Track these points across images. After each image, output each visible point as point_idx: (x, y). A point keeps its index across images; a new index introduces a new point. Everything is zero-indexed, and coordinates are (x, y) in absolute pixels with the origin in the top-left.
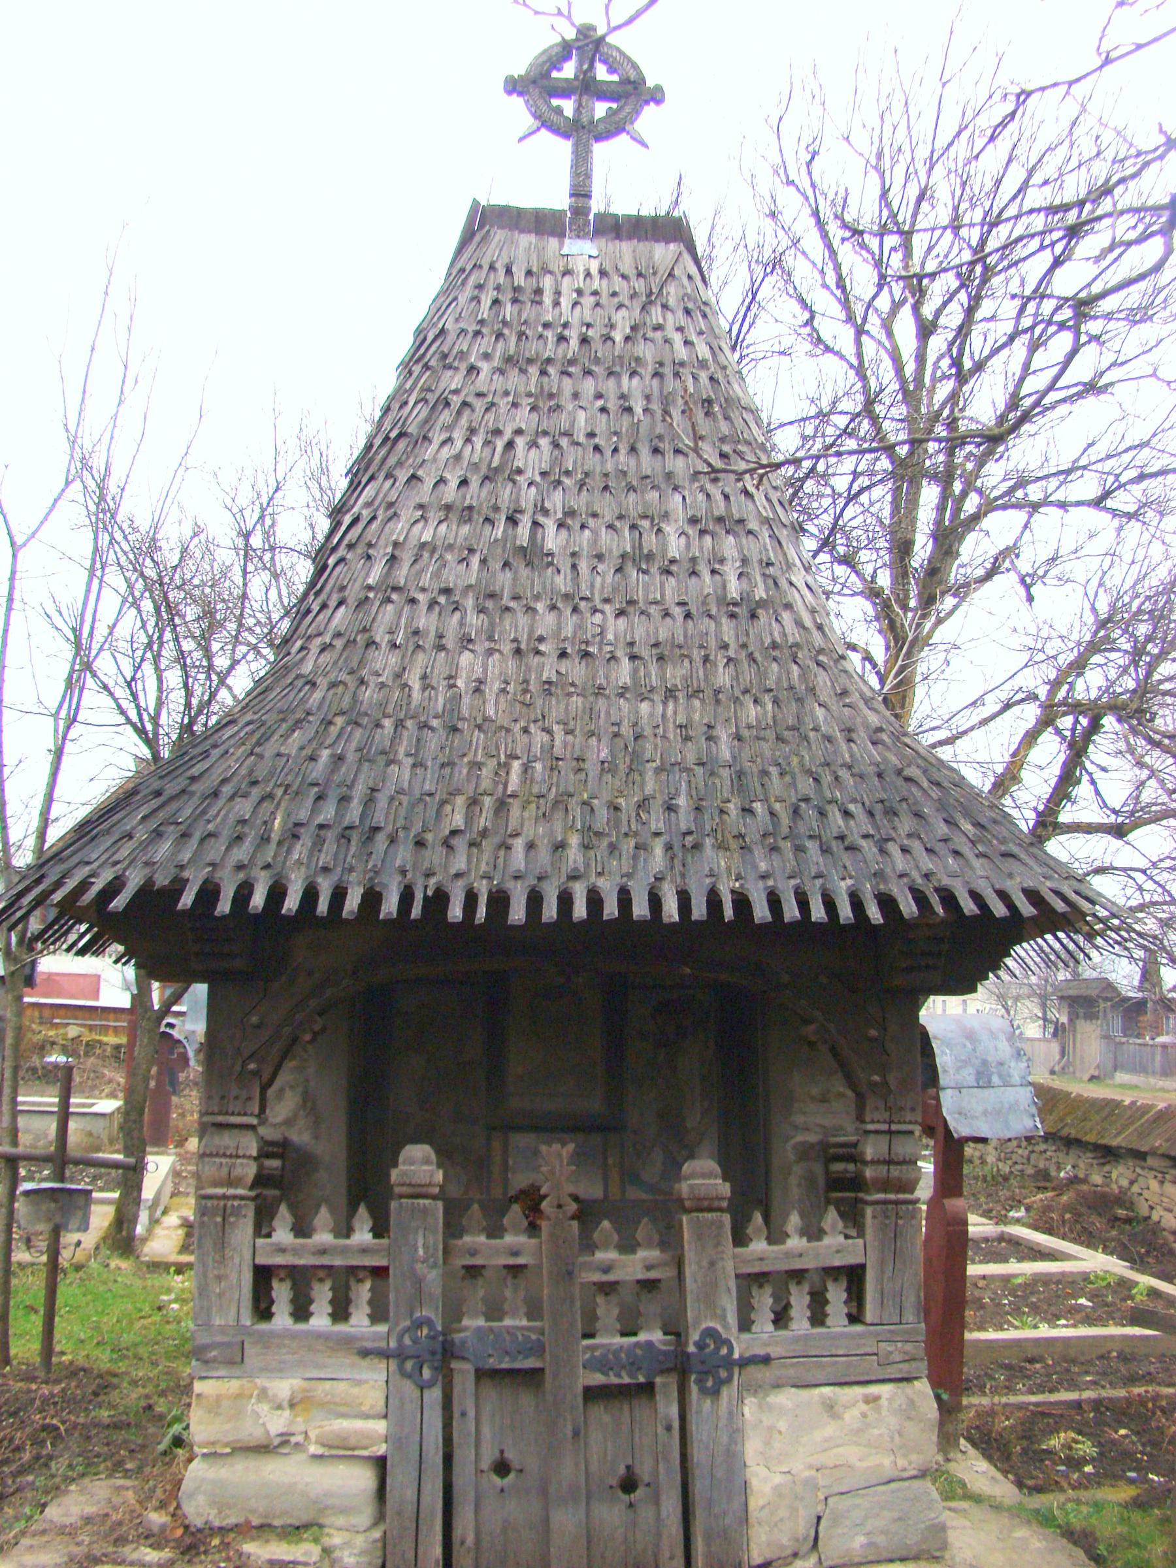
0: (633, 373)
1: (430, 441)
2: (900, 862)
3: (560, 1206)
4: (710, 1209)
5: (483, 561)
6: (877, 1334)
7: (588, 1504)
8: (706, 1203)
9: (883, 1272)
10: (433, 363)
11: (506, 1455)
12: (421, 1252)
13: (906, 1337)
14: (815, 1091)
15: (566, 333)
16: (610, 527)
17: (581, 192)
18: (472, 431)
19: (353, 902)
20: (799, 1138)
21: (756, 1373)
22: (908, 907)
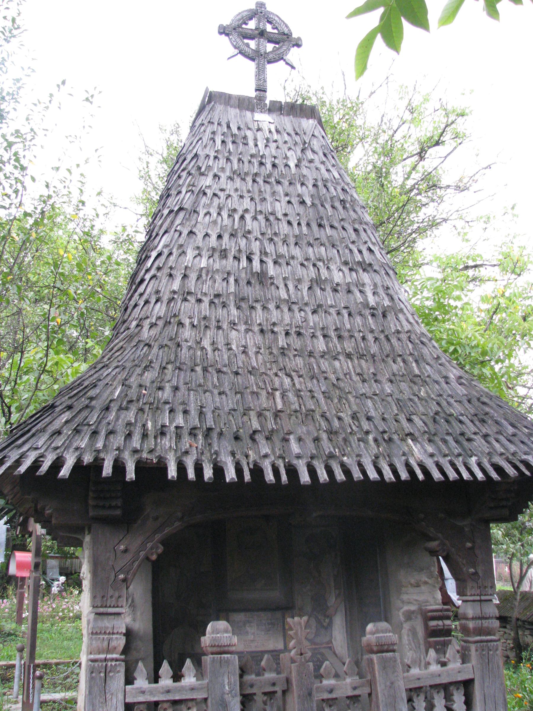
0: (302, 184)
4: (387, 651)
5: (236, 281)
8: (386, 647)
10: (193, 172)
12: (227, 688)
14: (413, 581)
15: (264, 161)
16: (302, 265)
17: (261, 89)
18: (220, 208)
20: (406, 608)
22: (511, 472)
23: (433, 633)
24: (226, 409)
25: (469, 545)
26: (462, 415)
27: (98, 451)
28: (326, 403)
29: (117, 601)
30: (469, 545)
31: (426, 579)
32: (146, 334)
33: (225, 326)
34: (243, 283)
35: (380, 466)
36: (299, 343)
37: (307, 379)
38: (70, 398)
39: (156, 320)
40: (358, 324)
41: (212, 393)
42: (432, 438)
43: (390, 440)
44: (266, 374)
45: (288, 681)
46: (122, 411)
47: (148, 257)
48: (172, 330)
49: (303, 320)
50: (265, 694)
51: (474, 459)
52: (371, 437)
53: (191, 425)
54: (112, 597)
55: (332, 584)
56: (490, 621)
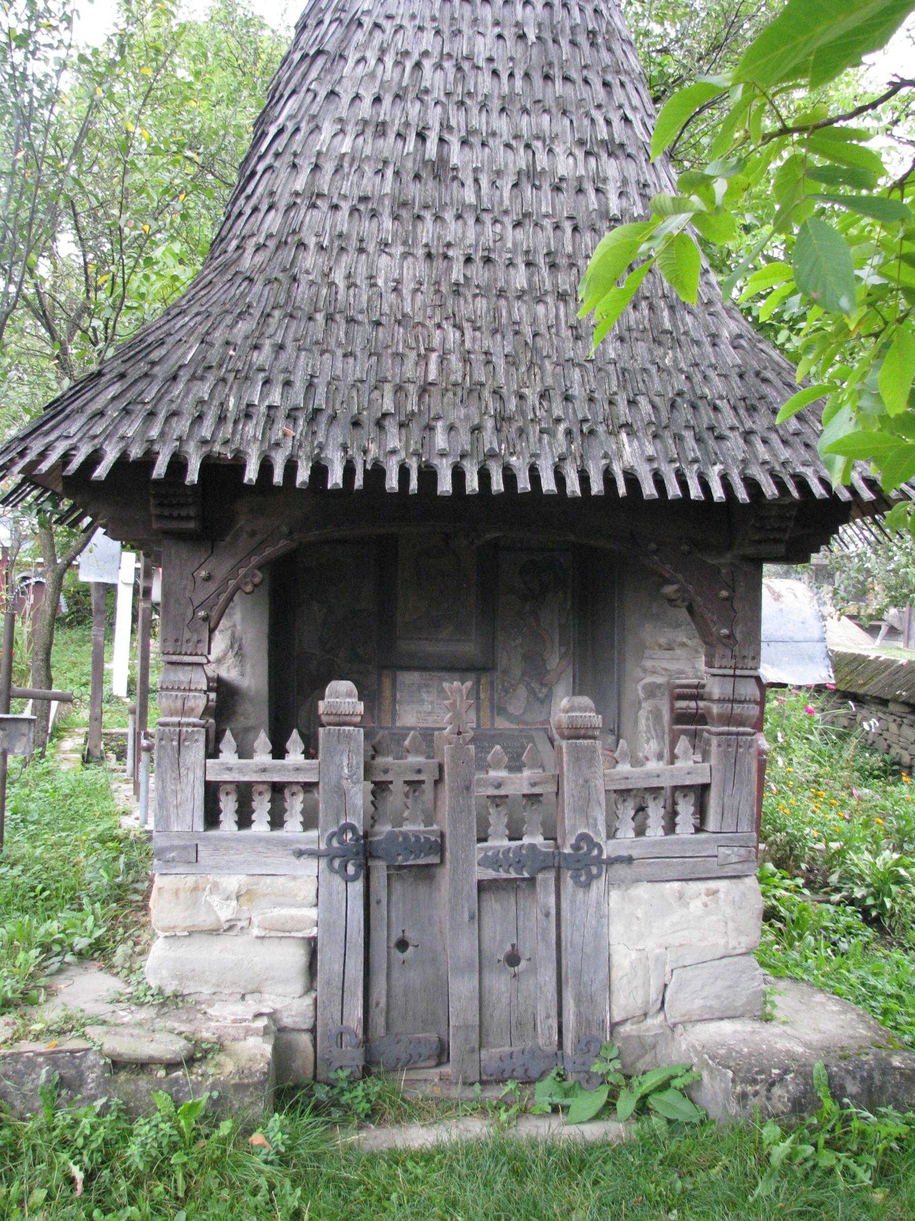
1: (346, 60)
2: (762, 452)
3: (459, 733)
4: (585, 737)
5: (397, 173)
6: (717, 840)
7: (480, 973)
8: (582, 732)
9: (724, 791)
11: (407, 934)
13: (742, 843)
14: (662, 641)
16: (508, 146)
18: (383, 51)
19: (303, 475)
20: (649, 679)
21: (620, 870)
22: (770, 490)
23: (680, 718)
24: (350, 380)
25: (724, 593)
26: (721, 398)
27: (152, 442)
28: (507, 372)
29: (196, 647)
30: (724, 593)
31: (685, 640)
32: (248, 261)
33: (371, 248)
34: (407, 177)
35: (564, 472)
36: (486, 274)
37: (487, 333)
38: (124, 362)
39: (266, 239)
40: (586, 246)
41: (333, 354)
42: (660, 432)
43: (592, 432)
44: (423, 325)
45: (441, 768)
46: (196, 382)
47: (264, 134)
48: (288, 254)
49: (498, 238)
50: (407, 783)
51: (718, 468)
52: (562, 428)
53: (290, 404)
54: (188, 641)
55: (557, 638)
56: (746, 706)
